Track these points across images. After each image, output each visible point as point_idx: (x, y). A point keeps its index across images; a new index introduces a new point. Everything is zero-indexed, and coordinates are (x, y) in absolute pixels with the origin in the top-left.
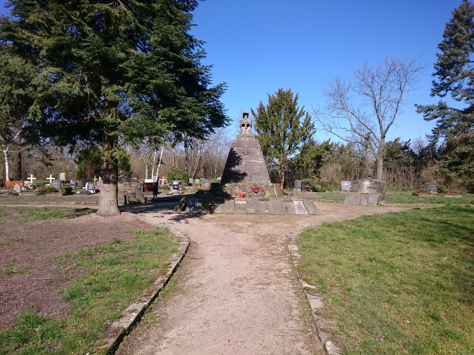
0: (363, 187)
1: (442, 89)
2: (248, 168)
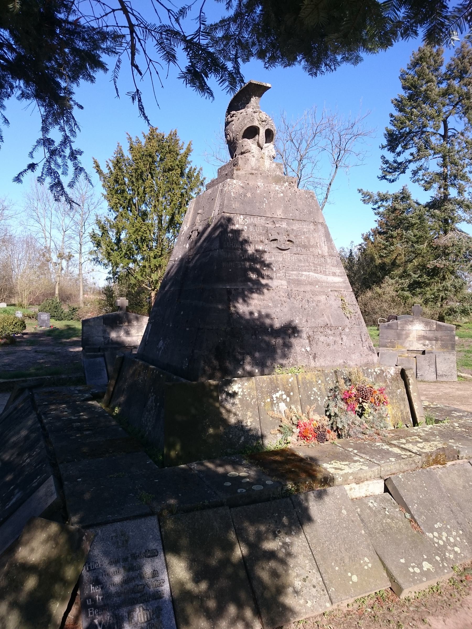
0: (407, 336)
1: (395, 170)
2: (297, 304)
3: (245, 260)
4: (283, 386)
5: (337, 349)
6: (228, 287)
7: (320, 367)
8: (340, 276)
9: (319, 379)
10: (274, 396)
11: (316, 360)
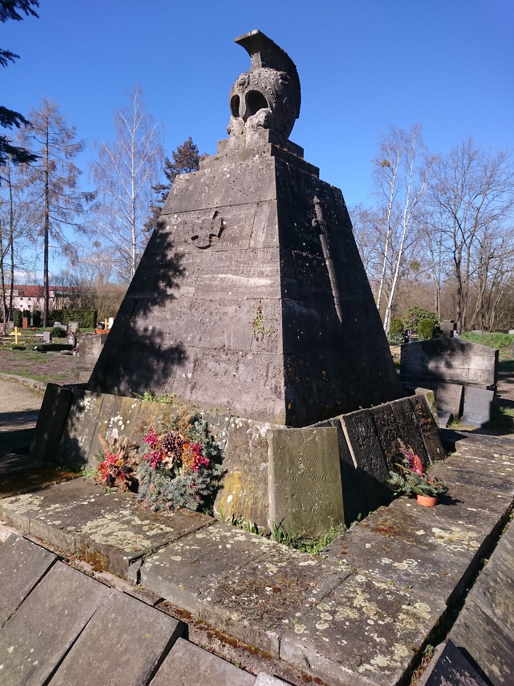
4: (124, 410)
6: (137, 297)
10: (112, 419)
11: (193, 391)
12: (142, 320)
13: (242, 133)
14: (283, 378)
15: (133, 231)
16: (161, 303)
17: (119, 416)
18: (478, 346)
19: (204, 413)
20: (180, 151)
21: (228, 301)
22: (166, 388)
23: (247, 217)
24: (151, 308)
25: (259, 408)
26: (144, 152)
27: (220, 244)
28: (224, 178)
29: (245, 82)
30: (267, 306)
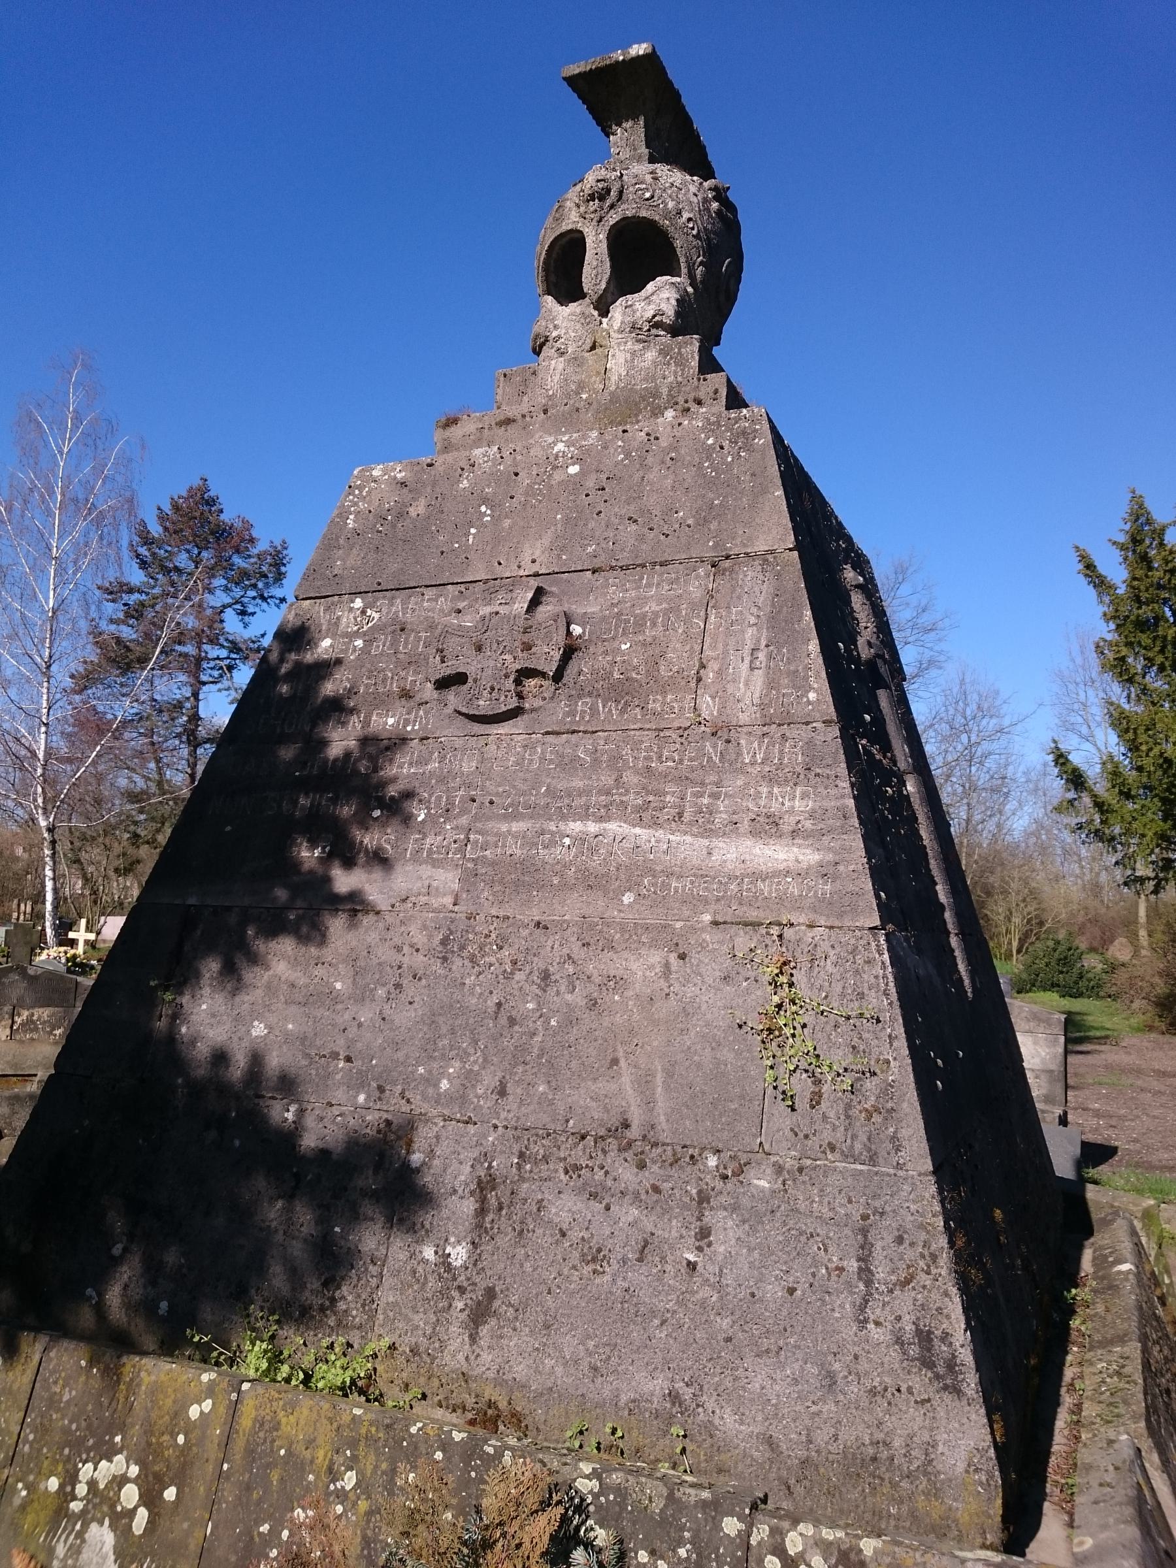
3: (304, 785)
4: (149, 1431)
5: (644, 1295)
6: (192, 901)
7: (499, 1382)
8: (808, 835)
9: (354, 1458)
10: (86, 1471)
11: (484, 1331)
12: (220, 998)
13: (593, 348)
14: (954, 1291)
15: (45, 691)
16: (304, 929)
17: (120, 1458)
18: (1020, 1007)
19: (594, 1484)
20: (176, 508)
21: (623, 930)
22: (342, 1306)
23: (674, 609)
24: (260, 946)
25: (848, 1436)
26: (87, 500)
27: (562, 707)
28: (558, 476)
29: (608, 191)
30: (819, 954)
